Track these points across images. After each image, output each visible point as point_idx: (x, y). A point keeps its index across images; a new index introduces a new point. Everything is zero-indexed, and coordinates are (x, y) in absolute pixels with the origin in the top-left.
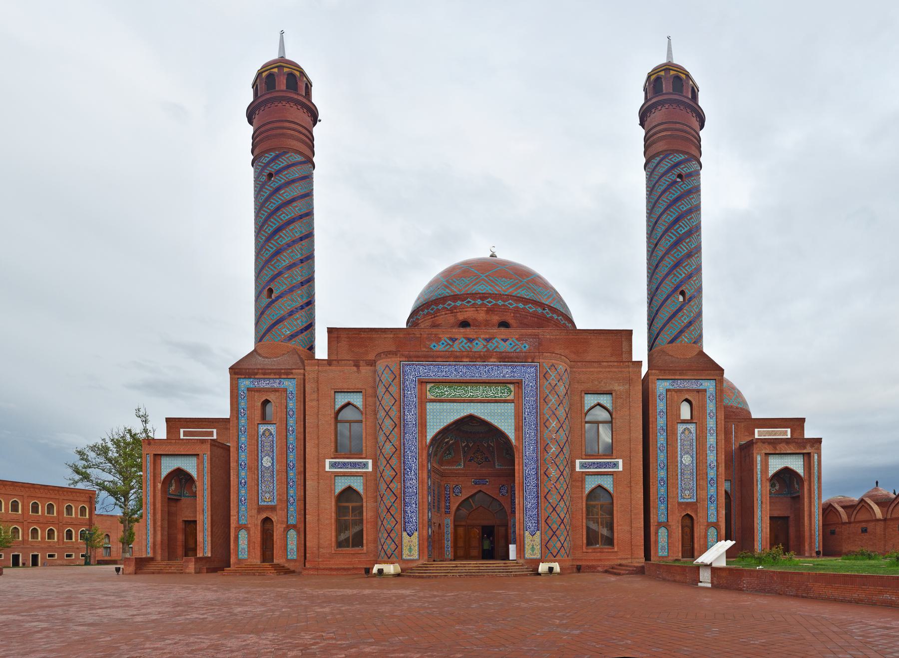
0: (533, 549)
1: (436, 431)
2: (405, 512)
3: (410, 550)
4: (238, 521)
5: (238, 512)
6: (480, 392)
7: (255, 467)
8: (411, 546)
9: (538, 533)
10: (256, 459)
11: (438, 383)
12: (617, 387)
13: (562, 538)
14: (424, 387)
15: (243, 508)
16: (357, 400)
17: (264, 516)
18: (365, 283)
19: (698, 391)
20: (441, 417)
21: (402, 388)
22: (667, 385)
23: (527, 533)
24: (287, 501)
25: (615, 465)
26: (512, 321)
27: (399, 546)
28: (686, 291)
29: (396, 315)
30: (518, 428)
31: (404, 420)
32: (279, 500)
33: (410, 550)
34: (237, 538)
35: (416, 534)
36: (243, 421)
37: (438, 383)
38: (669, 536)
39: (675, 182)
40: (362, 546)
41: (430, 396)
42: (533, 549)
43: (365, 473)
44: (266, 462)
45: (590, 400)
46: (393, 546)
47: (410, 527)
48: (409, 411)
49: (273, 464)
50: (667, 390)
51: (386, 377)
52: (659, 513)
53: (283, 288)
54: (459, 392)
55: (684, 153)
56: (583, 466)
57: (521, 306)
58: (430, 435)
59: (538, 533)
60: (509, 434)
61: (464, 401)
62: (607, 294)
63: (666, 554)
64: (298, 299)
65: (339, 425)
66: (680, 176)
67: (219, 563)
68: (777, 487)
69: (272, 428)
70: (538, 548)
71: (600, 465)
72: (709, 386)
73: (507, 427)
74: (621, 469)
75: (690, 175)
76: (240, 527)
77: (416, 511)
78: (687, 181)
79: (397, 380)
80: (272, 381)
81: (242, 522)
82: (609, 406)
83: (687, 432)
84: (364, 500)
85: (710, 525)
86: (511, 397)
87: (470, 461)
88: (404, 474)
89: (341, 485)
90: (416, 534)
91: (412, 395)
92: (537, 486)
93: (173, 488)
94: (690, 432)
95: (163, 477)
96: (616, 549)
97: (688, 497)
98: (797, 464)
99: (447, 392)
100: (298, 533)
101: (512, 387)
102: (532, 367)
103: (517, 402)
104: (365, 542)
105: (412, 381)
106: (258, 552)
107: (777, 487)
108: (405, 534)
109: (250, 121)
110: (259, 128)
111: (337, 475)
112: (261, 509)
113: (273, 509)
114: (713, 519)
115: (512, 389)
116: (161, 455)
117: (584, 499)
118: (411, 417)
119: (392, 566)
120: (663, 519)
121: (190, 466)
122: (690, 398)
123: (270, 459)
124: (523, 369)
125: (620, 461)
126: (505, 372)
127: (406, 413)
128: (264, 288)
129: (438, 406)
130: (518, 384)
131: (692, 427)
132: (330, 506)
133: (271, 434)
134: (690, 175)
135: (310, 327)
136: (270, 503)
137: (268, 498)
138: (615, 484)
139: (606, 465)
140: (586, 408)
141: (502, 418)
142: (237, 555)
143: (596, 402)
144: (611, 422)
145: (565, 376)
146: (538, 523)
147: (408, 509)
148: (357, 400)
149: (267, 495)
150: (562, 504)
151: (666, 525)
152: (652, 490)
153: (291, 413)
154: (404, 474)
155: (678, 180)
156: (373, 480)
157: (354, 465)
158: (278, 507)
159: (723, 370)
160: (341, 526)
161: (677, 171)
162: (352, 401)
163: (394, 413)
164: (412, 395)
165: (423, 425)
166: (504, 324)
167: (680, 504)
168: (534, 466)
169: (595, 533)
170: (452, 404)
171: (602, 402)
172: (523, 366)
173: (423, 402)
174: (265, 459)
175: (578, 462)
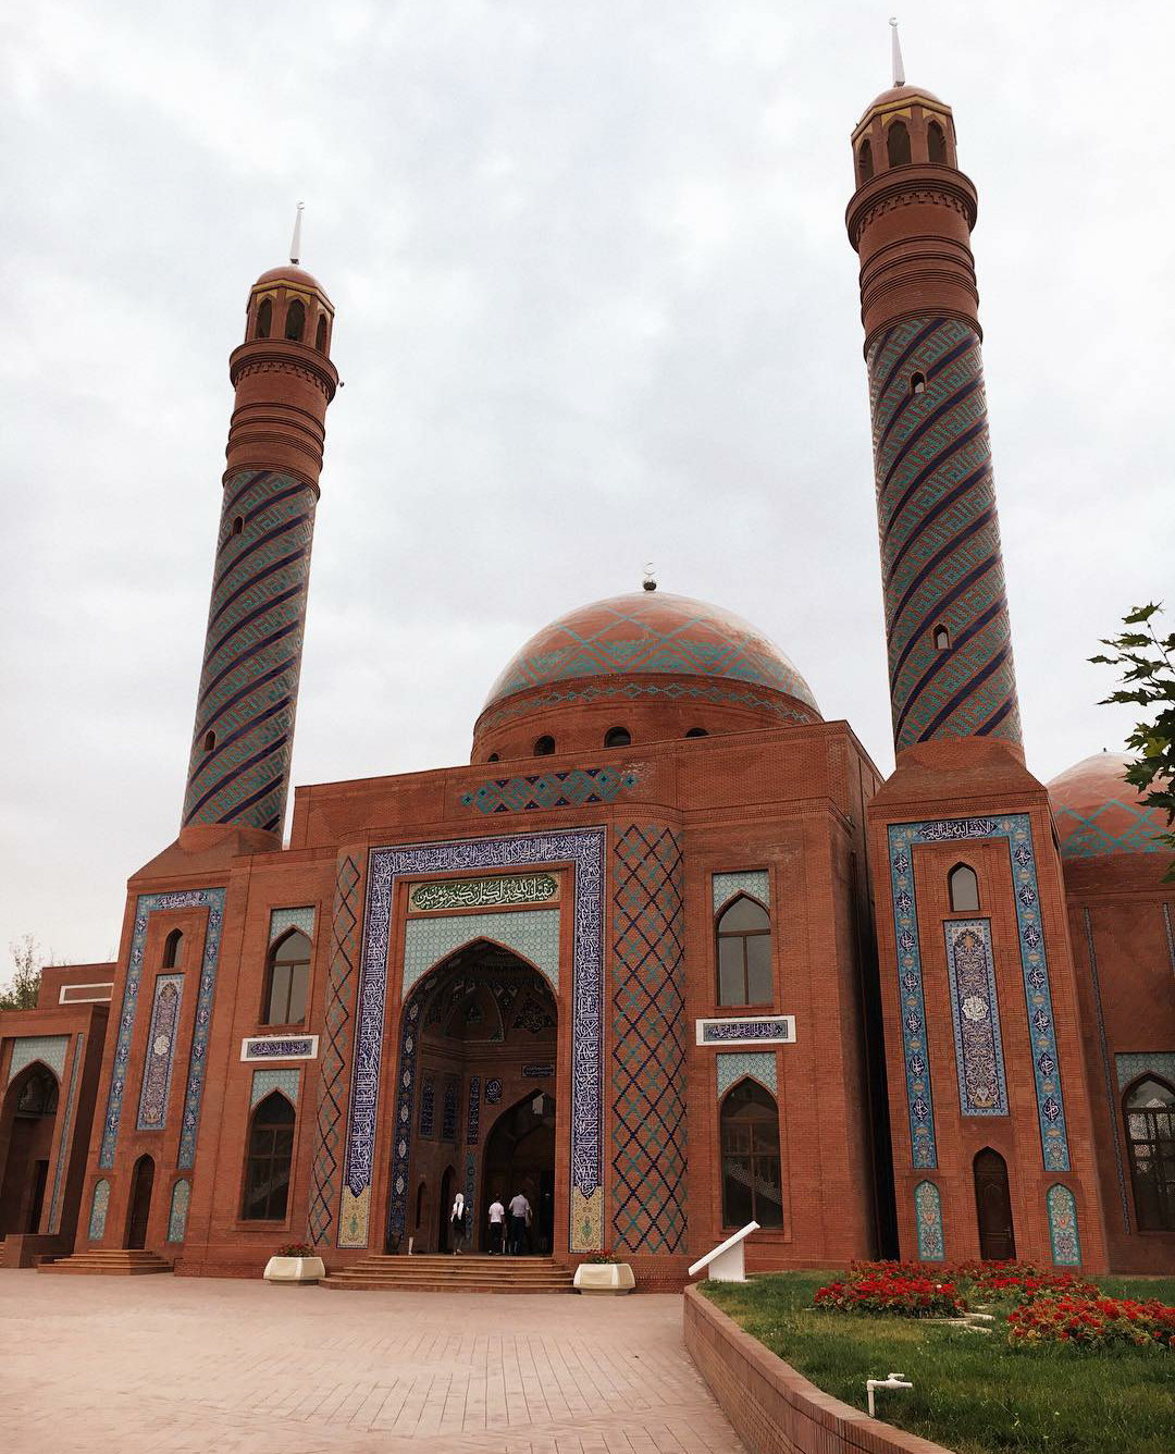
0: (587, 1229)
1: (420, 974)
2: (352, 1144)
4: (100, 1162)
5: (102, 1146)
6: (497, 894)
8: (357, 1217)
9: (599, 1191)
10: (147, 1040)
11: (429, 882)
13: (654, 1206)
14: (404, 891)
15: (110, 1138)
16: (306, 922)
18: (388, 696)
19: (986, 845)
20: (431, 943)
21: (369, 898)
22: (911, 834)
23: (576, 1192)
24: (184, 1121)
25: (781, 1029)
26: (632, 723)
27: (334, 1217)
29: (443, 741)
30: (567, 961)
31: (366, 957)
32: (171, 1120)
35: (367, 1191)
36: (135, 972)
37: (429, 882)
38: (944, 1209)
40: (283, 1216)
41: (414, 908)
42: (587, 1229)
43: (306, 1062)
44: (161, 1046)
45: (725, 888)
46: (325, 1217)
47: (359, 1175)
48: (376, 940)
49: (170, 1049)
50: (914, 848)
51: (346, 877)
52: (914, 1145)
53: (230, 731)
54: (463, 897)
55: (918, 314)
56: (710, 1033)
57: (653, 689)
58: (410, 980)
59: (599, 1191)
60: (549, 974)
61: (464, 914)
62: (848, 678)
64: (257, 740)
69: (177, 981)
70: (597, 1226)
71: (749, 1031)
72: (1016, 831)
74: (792, 1038)
76: (919, 1178)
77: (369, 1146)
79: (360, 884)
81: (106, 1164)
83: (968, 942)
84: (297, 1119)
85: (1053, 1180)
86: (555, 899)
87: (517, 1025)
88: (357, 1064)
89: (264, 1086)
90: (367, 1191)
91: (383, 907)
92: (599, 1082)
93: (28, 1097)
94: (978, 941)
96: (787, 1238)
97: (984, 1101)
99: (443, 897)
101: (557, 878)
102: (593, 834)
103: (567, 908)
104: (289, 1207)
105: (386, 881)
106: (121, 1228)
108: (347, 1191)
111: (258, 1068)
112: (138, 1137)
114: (1058, 1163)
115: (558, 882)
116: (15, 1038)
117: (715, 1111)
118: (377, 952)
119: (614, 1267)
123: (166, 1040)
124: (578, 841)
125: (791, 1020)
126: (545, 851)
127: (371, 944)
130: (568, 870)
133: (175, 993)
135: (281, 780)
138: (783, 1074)
139: (760, 1030)
141: (535, 940)
143: (736, 890)
145: (665, 846)
146: (599, 1168)
147: (358, 1138)
148: (306, 922)
150: (653, 1123)
151: (933, 1177)
152: (894, 1087)
153: (211, 951)
154: (357, 1064)
157: (288, 1048)
161: (908, 371)
162: (298, 924)
163: (351, 948)
164: (383, 907)
165: (397, 964)
166: (617, 736)
167: (966, 1123)
168: (593, 1038)
169: (746, 1191)
170: (449, 920)
172: (578, 834)
173: (401, 918)
174: (158, 1041)
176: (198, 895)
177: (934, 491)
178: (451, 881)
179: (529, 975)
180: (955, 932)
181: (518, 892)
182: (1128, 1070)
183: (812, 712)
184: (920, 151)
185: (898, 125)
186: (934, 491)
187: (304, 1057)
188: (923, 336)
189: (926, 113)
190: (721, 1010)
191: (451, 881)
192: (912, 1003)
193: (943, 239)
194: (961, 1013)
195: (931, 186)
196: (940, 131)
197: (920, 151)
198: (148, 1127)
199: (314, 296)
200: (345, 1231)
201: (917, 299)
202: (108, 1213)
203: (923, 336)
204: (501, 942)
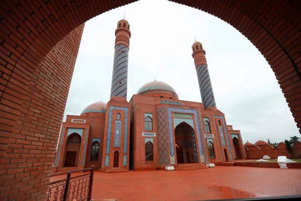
3: (173, 161)
6: (185, 116)
7: (113, 134)
12: (209, 116)
16: (151, 116)
17: (116, 150)
20: (177, 122)
28: (121, 82)
30: (195, 126)
33: (173, 161)
34: (105, 158)
35: (174, 156)
37: (176, 113)
39: (121, 54)
41: (174, 116)
44: (117, 132)
47: (172, 154)
48: (170, 120)
49: (119, 133)
55: (200, 64)
56: (144, 134)
59: (203, 155)
62: (189, 92)
63: (204, 162)
65: (147, 122)
66: (123, 52)
67: (131, 166)
68: (77, 140)
70: (204, 160)
71: (209, 136)
73: (192, 125)
75: (125, 52)
78: (124, 53)
80: (121, 108)
82: (151, 117)
95: (68, 136)
96: (217, 159)
98: (236, 136)
100: (127, 156)
103: (193, 119)
107: (77, 140)
109: (193, 57)
110: (196, 59)
112: (115, 148)
113: (119, 148)
120: (108, 152)
121: (80, 132)
122: (119, 112)
123: (118, 131)
126: (190, 111)
128: (119, 81)
129: (176, 119)
131: (120, 122)
132: (143, 147)
134: (125, 52)
136: (118, 146)
137: (117, 143)
140: (145, 117)
141: (190, 123)
142: (105, 164)
144: (152, 122)
149: (117, 143)
155: (122, 53)
156: (157, 139)
158: (121, 148)
159: (223, 115)
160: (147, 153)
161: (122, 50)
171: (150, 116)
175: (143, 133)
176: (122, 108)
177: (204, 82)
178: (179, 113)
179: (189, 126)
180: (117, 122)
181: (188, 116)
182: (94, 140)
183: (178, 98)
184: (200, 48)
185: (197, 45)
186: (204, 82)
187: (153, 136)
188: (201, 66)
189: (123, 22)
190: (207, 134)
191: (179, 113)
192: (109, 130)
193: (203, 57)
194: (116, 133)
195: (125, 30)
196: (201, 46)
197: (200, 48)
198: (116, 146)
199: (127, 22)
200: (171, 162)
201: (201, 62)
202: (109, 161)
203: (201, 66)
204: (186, 122)
